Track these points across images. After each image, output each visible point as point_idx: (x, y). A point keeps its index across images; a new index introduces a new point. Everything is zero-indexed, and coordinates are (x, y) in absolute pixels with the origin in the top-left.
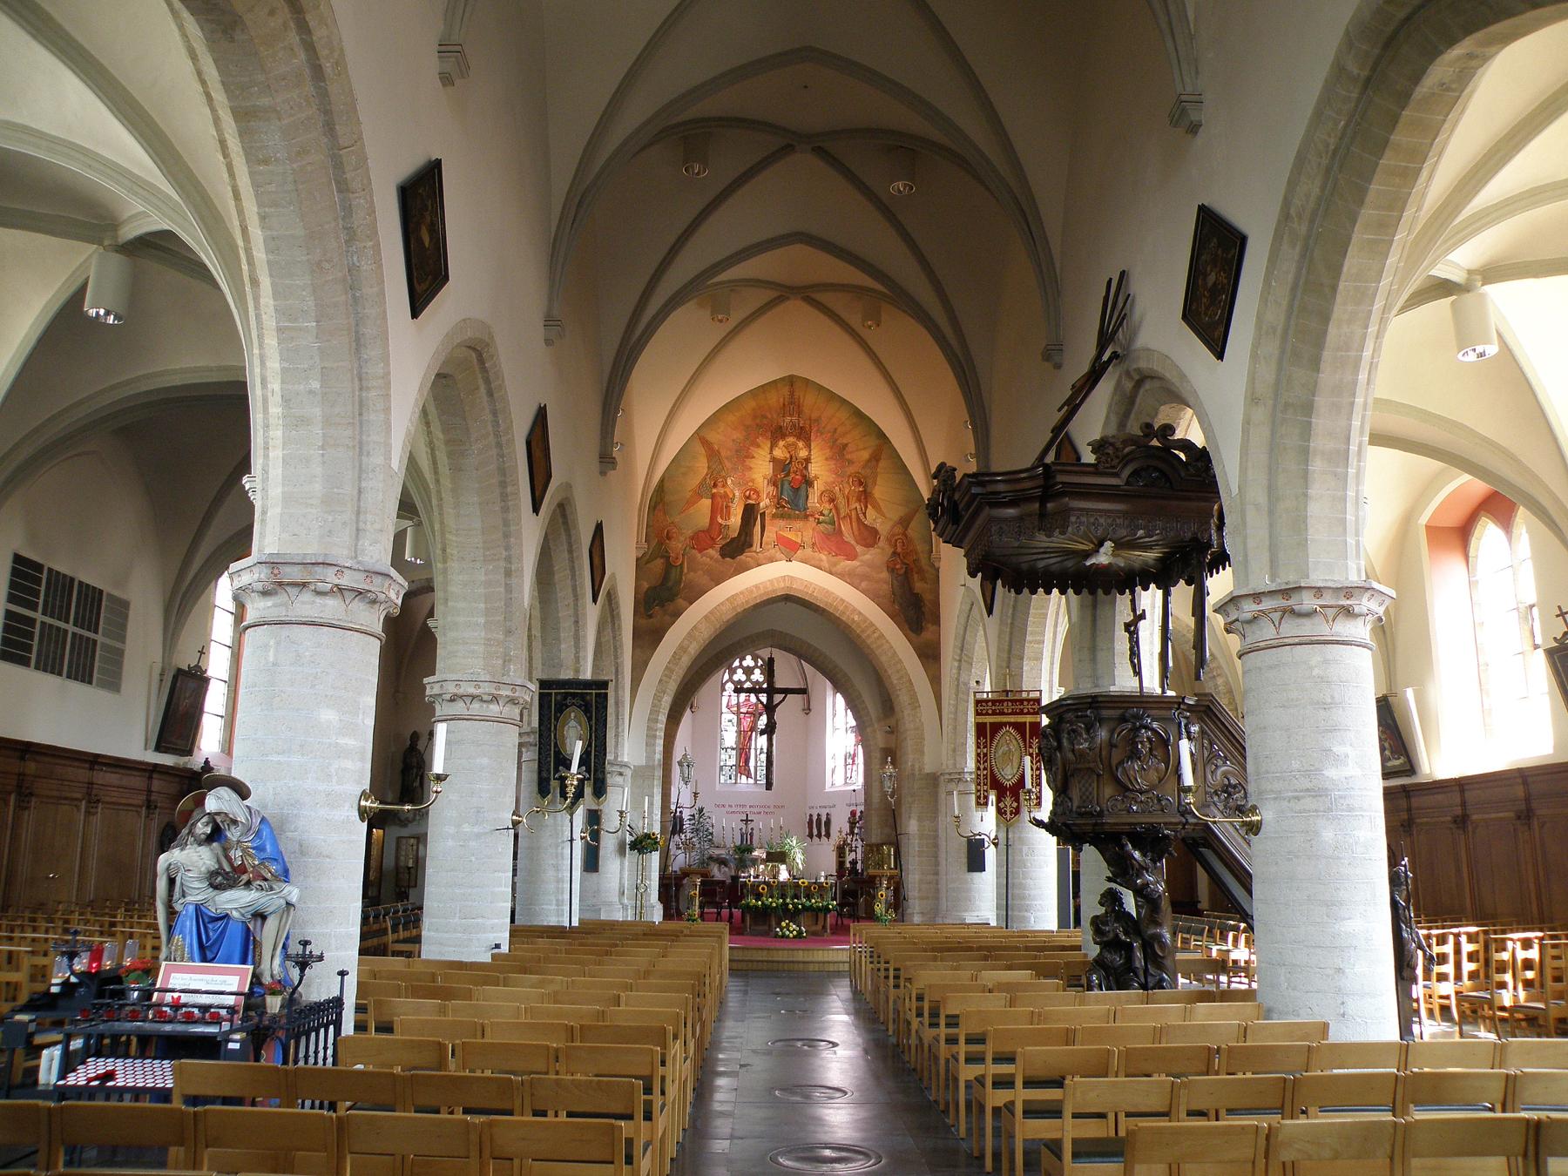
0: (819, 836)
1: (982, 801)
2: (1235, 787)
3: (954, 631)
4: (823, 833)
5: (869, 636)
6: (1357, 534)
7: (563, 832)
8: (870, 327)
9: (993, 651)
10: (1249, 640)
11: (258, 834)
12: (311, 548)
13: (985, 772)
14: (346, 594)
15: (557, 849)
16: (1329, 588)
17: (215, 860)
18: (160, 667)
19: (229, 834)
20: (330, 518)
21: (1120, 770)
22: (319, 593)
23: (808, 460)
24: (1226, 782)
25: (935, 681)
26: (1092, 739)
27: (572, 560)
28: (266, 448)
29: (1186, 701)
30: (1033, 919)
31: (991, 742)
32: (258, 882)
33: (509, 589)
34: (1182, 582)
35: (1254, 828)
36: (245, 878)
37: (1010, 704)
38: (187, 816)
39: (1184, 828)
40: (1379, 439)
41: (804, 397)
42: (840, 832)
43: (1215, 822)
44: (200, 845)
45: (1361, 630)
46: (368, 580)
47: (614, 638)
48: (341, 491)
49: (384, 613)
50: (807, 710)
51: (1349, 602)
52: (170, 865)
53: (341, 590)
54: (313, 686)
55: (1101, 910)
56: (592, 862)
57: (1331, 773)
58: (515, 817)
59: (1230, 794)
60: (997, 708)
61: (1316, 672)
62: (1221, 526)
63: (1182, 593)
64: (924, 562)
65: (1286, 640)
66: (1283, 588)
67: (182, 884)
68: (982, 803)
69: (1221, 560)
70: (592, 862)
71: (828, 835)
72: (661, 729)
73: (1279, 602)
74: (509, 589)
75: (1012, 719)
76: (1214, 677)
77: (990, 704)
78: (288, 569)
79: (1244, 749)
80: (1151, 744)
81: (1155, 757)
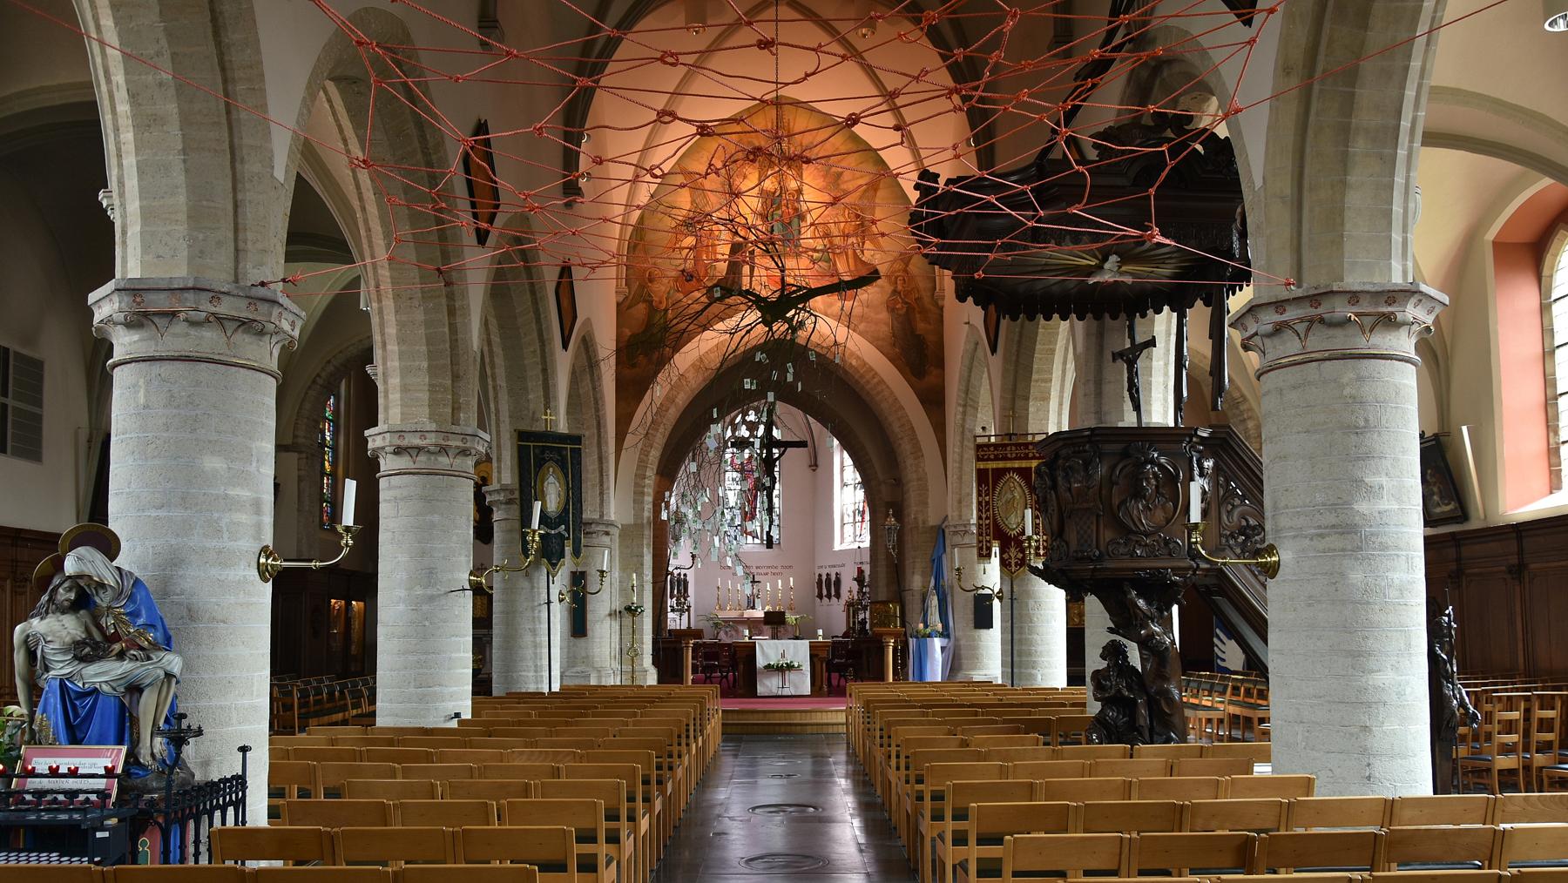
0: (829, 596)
1: (984, 552)
2: (1254, 528)
3: (957, 375)
4: (833, 593)
5: (878, 393)
6: (1405, 230)
7: (539, 594)
8: (864, 36)
9: (997, 393)
10: (1270, 357)
11: (131, 598)
12: (179, 271)
13: (987, 522)
14: (226, 323)
15: (533, 611)
16: (1368, 292)
17: (83, 629)
18: (87, 431)
19: (97, 600)
20: (201, 236)
21: (1123, 508)
22: (194, 324)
23: (799, 191)
24: (1244, 523)
25: (940, 428)
26: (1089, 477)
27: (535, 302)
28: (119, 156)
29: (1199, 433)
30: (1039, 677)
31: (994, 489)
32: (132, 652)
33: (453, 329)
34: (1199, 303)
35: (1272, 570)
36: (117, 647)
37: (1014, 448)
38: (44, 583)
39: (1194, 574)
40: (1434, 138)
41: (795, 120)
42: (850, 591)
43: (1225, 564)
44: (63, 613)
45: (1405, 343)
46: (252, 308)
47: (594, 389)
48: (212, 204)
49: (279, 346)
50: (814, 465)
51: (1390, 309)
52: (28, 636)
53: (220, 320)
54: (193, 430)
55: (1103, 664)
56: (579, 626)
57: (1362, 507)
58: (472, 578)
59: (1248, 537)
60: (1000, 452)
61: (1347, 391)
62: (1243, 235)
63: (1199, 314)
64: (927, 300)
65: (1313, 355)
66: (1311, 293)
67: (43, 657)
68: (985, 555)
69: (1244, 277)
70: (579, 626)
71: (838, 596)
72: (649, 486)
73: (1307, 311)
74: (453, 329)
75: (1017, 464)
76: (1244, 420)
77: (992, 449)
78: (152, 297)
79: (1262, 482)
80: (1157, 481)
81: (1163, 496)
